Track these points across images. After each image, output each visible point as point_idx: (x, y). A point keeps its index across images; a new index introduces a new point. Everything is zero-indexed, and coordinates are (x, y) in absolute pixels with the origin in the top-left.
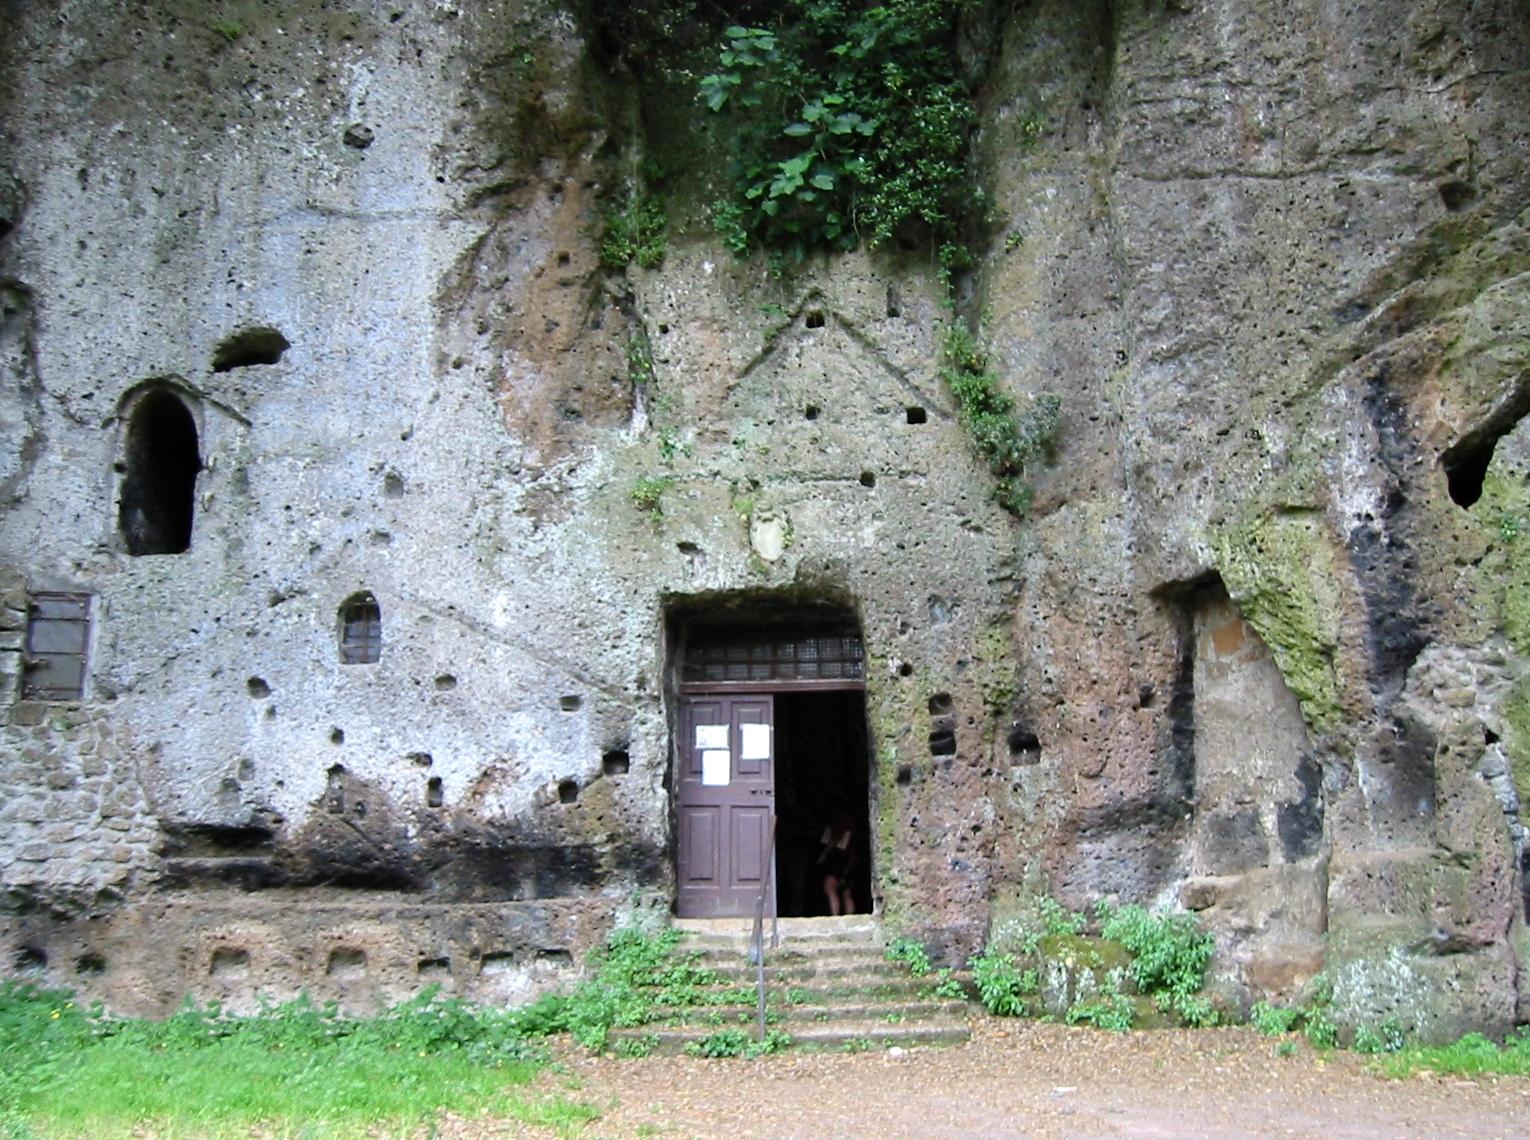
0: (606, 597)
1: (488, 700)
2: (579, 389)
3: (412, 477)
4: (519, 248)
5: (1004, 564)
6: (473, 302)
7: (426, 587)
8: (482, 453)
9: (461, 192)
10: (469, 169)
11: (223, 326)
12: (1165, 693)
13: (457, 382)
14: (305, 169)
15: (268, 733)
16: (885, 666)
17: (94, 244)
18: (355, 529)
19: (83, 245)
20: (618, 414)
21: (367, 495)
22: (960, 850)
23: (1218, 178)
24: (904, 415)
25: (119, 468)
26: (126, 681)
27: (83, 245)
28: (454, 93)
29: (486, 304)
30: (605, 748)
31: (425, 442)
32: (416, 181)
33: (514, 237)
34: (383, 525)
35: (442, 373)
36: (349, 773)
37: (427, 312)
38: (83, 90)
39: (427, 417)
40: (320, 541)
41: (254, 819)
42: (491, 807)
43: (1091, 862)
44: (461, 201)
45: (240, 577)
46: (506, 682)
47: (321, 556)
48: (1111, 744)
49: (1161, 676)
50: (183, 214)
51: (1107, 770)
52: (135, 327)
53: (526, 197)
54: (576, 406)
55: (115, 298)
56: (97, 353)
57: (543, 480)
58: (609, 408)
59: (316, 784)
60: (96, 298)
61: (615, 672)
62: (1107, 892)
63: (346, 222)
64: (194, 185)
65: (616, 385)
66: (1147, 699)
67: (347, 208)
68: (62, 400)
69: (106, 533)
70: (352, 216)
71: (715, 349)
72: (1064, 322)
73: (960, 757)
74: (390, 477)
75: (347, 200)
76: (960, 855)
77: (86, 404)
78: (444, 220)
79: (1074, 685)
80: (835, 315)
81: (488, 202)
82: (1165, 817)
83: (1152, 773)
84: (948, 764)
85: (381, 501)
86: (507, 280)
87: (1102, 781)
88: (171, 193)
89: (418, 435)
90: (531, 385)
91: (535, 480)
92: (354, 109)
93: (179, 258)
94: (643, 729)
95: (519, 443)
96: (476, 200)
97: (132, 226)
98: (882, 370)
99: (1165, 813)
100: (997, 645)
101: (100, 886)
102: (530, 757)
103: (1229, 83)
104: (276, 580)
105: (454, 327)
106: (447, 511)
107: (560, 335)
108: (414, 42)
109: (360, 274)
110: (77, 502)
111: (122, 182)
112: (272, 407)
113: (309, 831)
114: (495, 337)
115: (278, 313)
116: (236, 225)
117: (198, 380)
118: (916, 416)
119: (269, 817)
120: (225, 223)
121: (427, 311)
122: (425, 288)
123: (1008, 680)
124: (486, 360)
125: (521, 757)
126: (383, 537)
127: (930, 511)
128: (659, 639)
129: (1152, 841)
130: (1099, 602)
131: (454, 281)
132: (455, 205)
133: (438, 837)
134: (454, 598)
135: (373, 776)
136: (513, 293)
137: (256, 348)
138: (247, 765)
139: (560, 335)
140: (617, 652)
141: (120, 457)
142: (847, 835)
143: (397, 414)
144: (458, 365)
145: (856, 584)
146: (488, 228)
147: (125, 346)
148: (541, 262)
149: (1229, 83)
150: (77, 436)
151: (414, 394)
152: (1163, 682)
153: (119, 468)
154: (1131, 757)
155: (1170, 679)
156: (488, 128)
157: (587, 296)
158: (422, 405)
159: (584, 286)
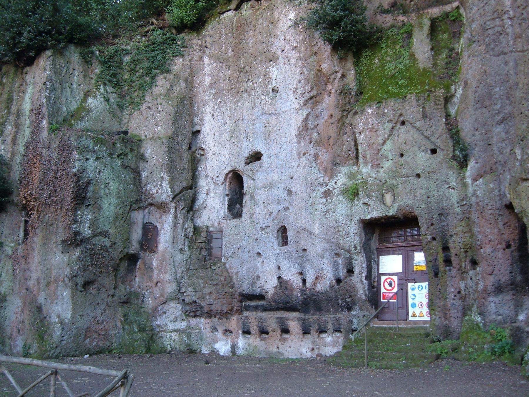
0: (344, 222)
1: (315, 255)
2: (339, 156)
3: (293, 190)
4: (321, 114)
5: (462, 200)
6: (308, 134)
7: (298, 223)
8: (311, 181)
9: (302, 100)
10: (304, 93)
11: (246, 152)
12: (515, 243)
13: (304, 159)
14: (263, 102)
15: (262, 268)
16: (427, 238)
17: (217, 134)
18: (280, 207)
19: (214, 135)
20: (352, 162)
21: (283, 196)
22: (454, 299)
23: (510, 54)
24: (429, 152)
25: (228, 195)
26: (230, 254)
27: (214, 135)
28: (298, 71)
29: (312, 133)
30: (347, 269)
31: (296, 179)
32: (290, 100)
33: (319, 110)
34: (287, 205)
35: (299, 158)
36: (283, 278)
37: (295, 140)
38: (211, 91)
39: (297, 172)
40: (272, 211)
41: (261, 292)
42: (319, 287)
43: (493, 305)
44: (302, 103)
45: (255, 223)
46: (319, 250)
47: (272, 216)
48: (495, 263)
49: (513, 237)
50: (236, 122)
51: (494, 272)
52: (227, 156)
53: (321, 98)
54: (338, 161)
55: (222, 148)
56: (219, 164)
57: (328, 187)
58: (349, 160)
59: (274, 282)
60: (218, 149)
61: (348, 245)
62: (499, 315)
63: (274, 116)
64: (237, 113)
65: (350, 152)
66: (508, 246)
67: (274, 112)
68: (213, 178)
69: (225, 214)
70: (275, 114)
71: (374, 138)
72: (480, 110)
73: (454, 267)
74: (288, 190)
75: (274, 109)
76: (454, 302)
77: (217, 179)
78: (298, 110)
79: (484, 242)
80: (407, 121)
81: (310, 102)
82: (518, 288)
83: (511, 273)
84: (450, 270)
85: (286, 198)
86: (318, 125)
87: (493, 276)
88: (232, 117)
89: (295, 177)
90: (325, 157)
91: (326, 186)
92: (274, 82)
93: (235, 135)
94: (357, 262)
95: (323, 175)
96: (306, 102)
97: (224, 127)
98: (422, 137)
99: (518, 287)
100: (463, 228)
101: (225, 311)
102: (327, 272)
103: (509, 18)
104: (262, 224)
105: (302, 143)
106: (302, 199)
107: (332, 140)
108: (287, 57)
109: (278, 131)
110: (217, 206)
111: (221, 115)
112: (259, 174)
113: (274, 295)
114: (314, 144)
115: (260, 147)
116: (248, 122)
117: (241, 169)
118: (434, 151)
119: (264, 292)
120: (246, 122)
121: (295, 139)
122: (294, 133)
123: (467, 240)
124: (312, 151)
125: (325, 272)
126: (287, 208)
127: (437, 184)
128: (360, 234)
129: (514, 297)
130: (490, 212)
131: (301, 129)
132: (300, 105)
133: (305, 296)
134: (305, 225)
135: (288, 279)
136: (321, 128)
137: (256, 157)
138: (258, 277)
139: (332, 140)
140: (348, 239)
141: (227, 192)
142: (395, 301)
143: (290, 171)
144: (304, 154)
145: (417, 212)
146: (310, 110)
147: (225, 161)
148: (326, 118)
149: (509, 18)
150: (217, 187)
151: (293, 165)
152: (514, 239)
153: (228, 195)
154: (503, 267)
155: (517, 238)
156: (307, 79)
157: (339, 126)
158: (295, 168)
159: (338, 123)
